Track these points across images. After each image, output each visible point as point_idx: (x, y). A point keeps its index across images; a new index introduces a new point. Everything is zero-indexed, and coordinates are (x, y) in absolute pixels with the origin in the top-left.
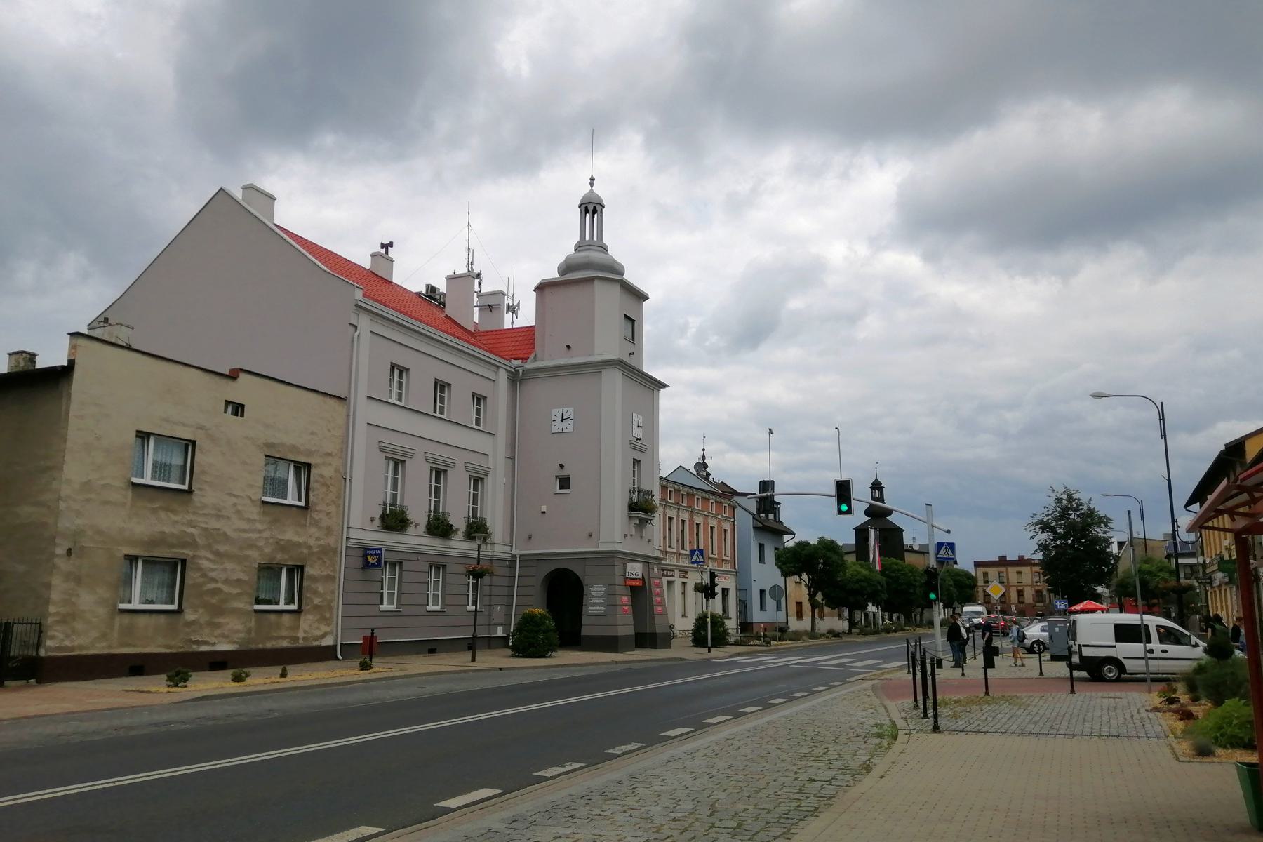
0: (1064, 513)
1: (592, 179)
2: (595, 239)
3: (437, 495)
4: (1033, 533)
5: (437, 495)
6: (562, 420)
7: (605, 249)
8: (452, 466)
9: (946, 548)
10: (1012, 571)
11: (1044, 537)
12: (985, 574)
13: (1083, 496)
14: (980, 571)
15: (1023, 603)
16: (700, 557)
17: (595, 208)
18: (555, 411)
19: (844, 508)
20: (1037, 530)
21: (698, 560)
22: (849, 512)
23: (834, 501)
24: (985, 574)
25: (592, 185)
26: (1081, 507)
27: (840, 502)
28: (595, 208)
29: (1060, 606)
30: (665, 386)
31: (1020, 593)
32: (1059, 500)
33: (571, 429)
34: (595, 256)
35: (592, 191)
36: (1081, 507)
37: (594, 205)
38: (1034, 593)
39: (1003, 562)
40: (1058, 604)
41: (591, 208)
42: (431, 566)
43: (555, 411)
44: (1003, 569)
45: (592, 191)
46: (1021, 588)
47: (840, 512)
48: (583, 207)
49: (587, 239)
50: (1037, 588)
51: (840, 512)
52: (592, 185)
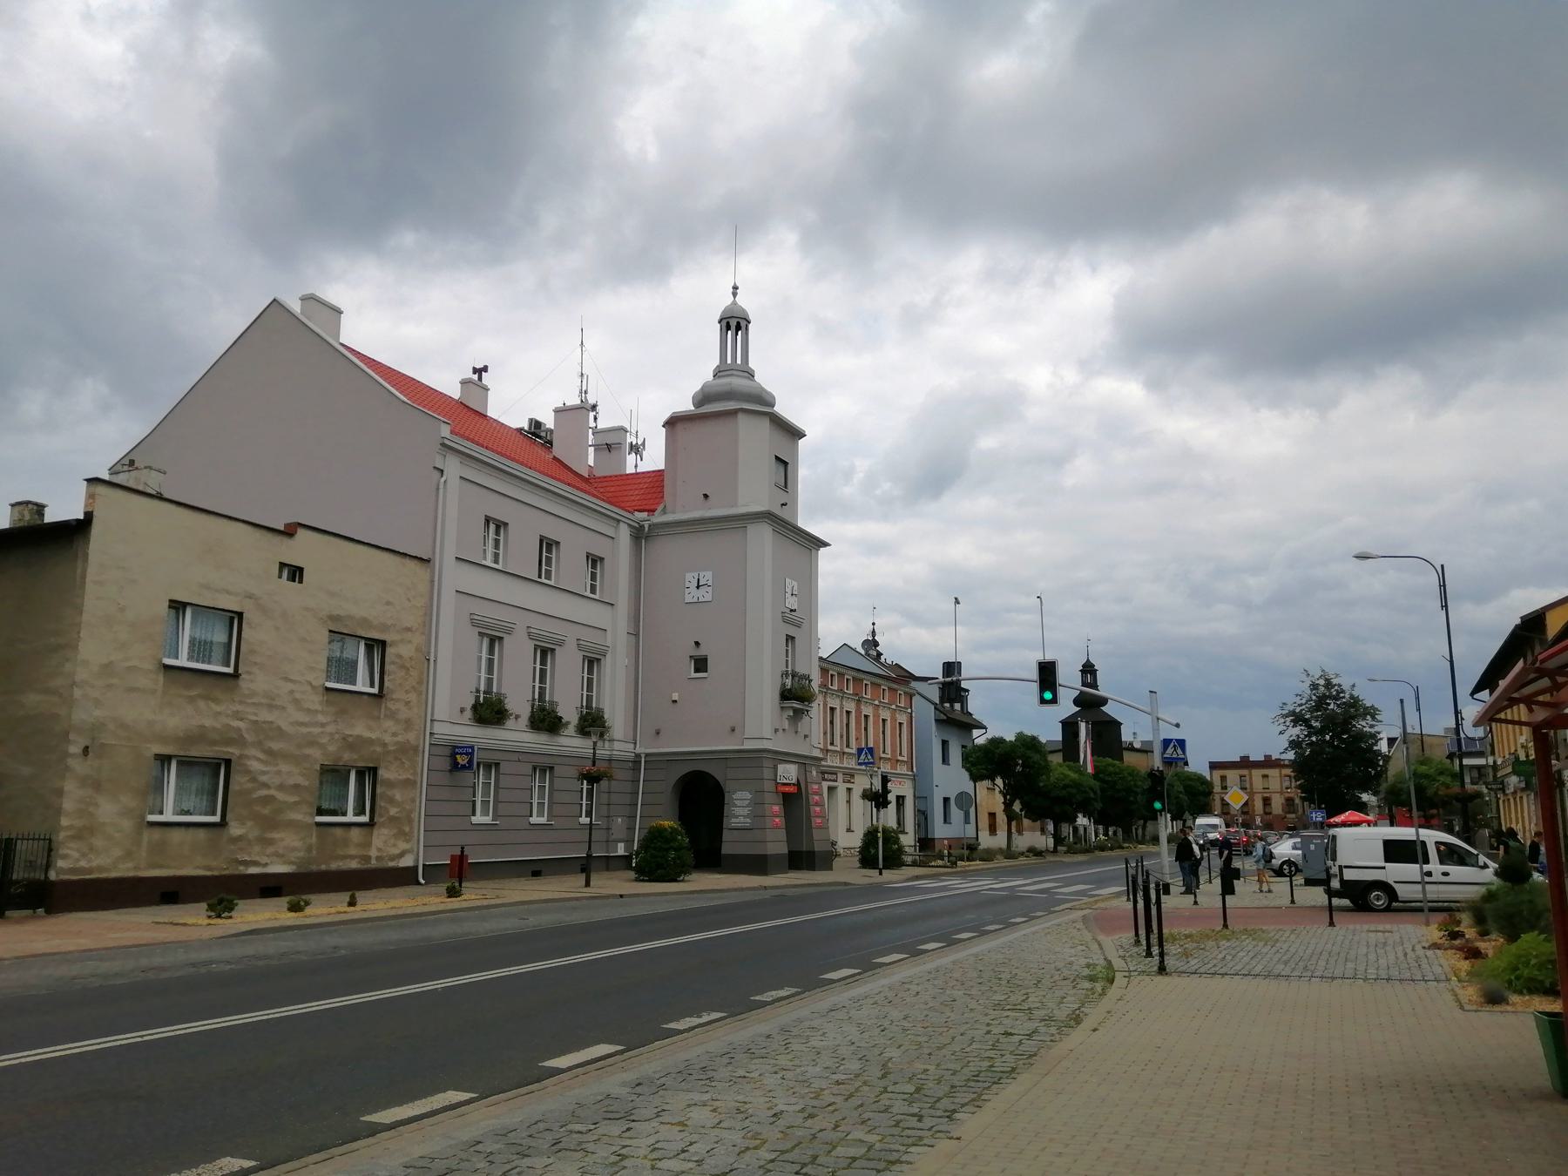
0: (1321, 703)
2: (739, 362)
3: (542, 680)
4: (1282, 728)
5: (542, 680)
6: (698, 587)
7: (751, 375)
8: (561, 643)
10: (1257, 774)
11: (1296, 731)
12: (1223, 778)
13: (1345, 682)
16: (869, 757)
17: (738, 323)
18: (689, 576)
19: (1048, 696)
20: (1288, 724)
21: (866, 761)
22: (1054, 701)
23: (1035, 687)
25: (735, 294)
26: (1342, 695)
27: (1042, 689)
28: (738, 323)
30: (825, 544)
31: (1267, 802)
32: (1314, 686)
33: (708, 597)
34: (738, 382)
35: (734, 303)
36: (1342, 695)
38: (1284, 802)
40: (1314, 815)
41: (733, 324)
42: (535, 769)
43: (689, 576)
45: (734, 303)
46: (1268, 795)
47: (1043, 701)
48: (724, 323)
49: (729, 361)
50: (1287, 795)
51: (1043, 701)
52: (735, 294)
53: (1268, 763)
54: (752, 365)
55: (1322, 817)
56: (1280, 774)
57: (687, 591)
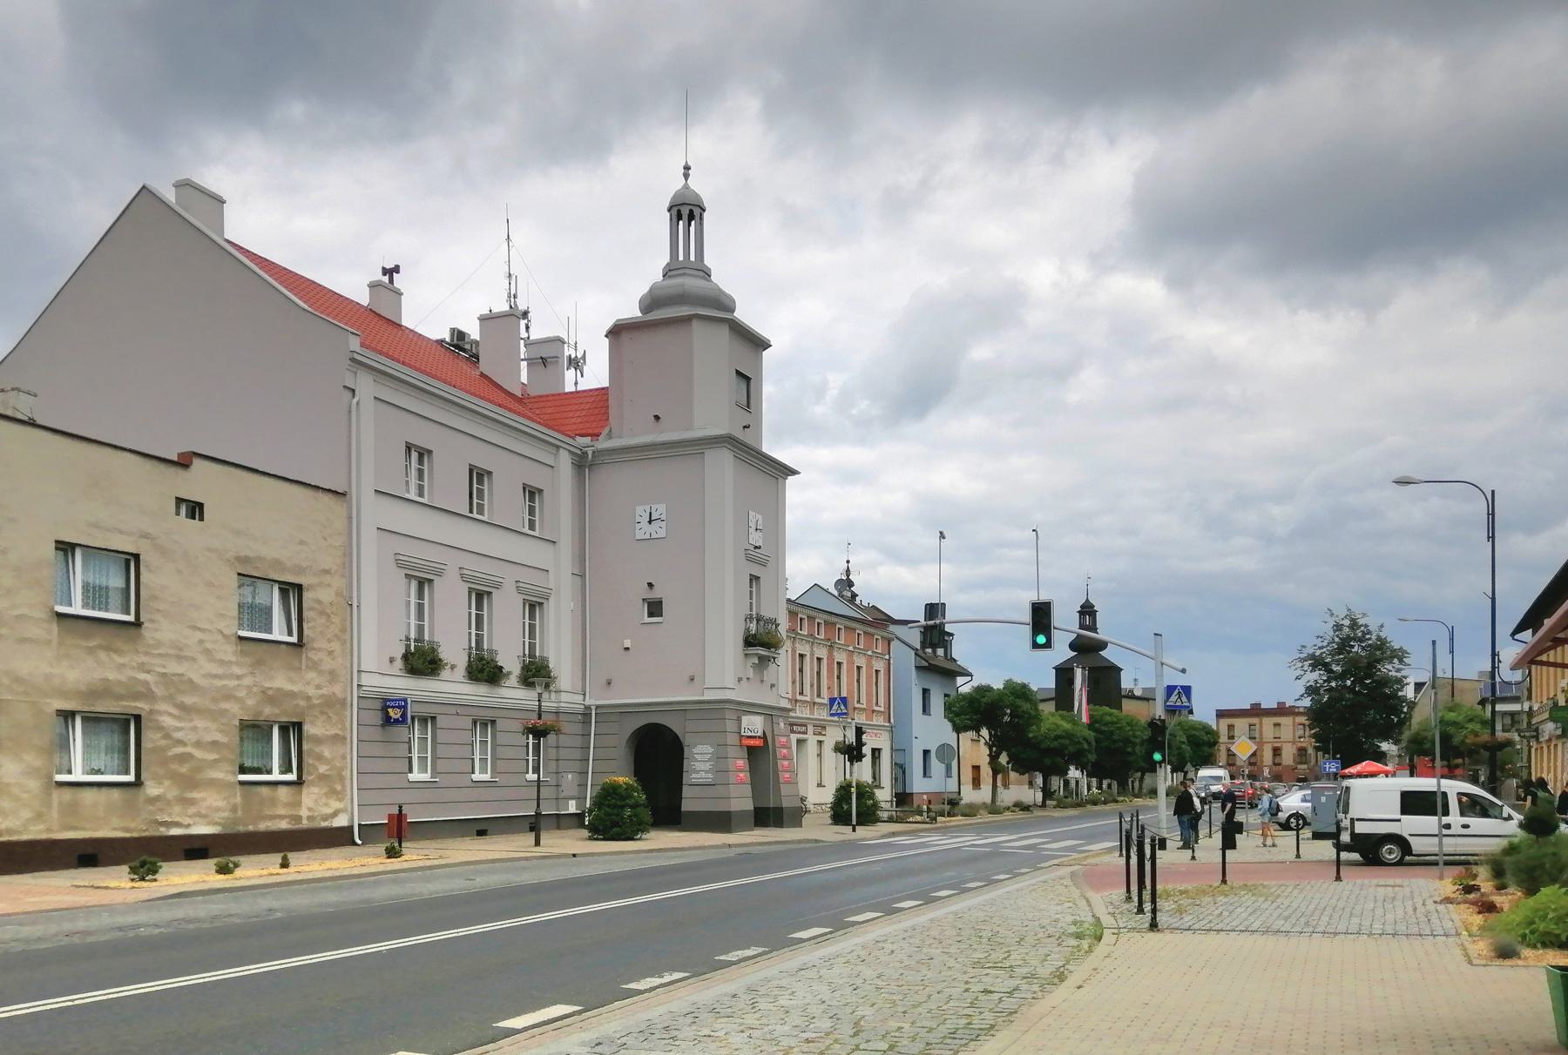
0: (1344, 645)
1: (687, 168)
2: (692, 258)
4: (1299, 672)
6: (650, 522)
7: (706, 274)
9: (839, 703)
10: (1268, 722)
11: (1315, 676)
12: (1231, 727)
14: (1225, 722)
15: (1280, 764)
16: (843, 707)
18: (639, 510)
19: (1041, 639)
20: (1305, 668)
22: (1048, 645)
23: (1028, 630)
24: (1231, 727)
25: (686, 176)
26: (1368, 636)
27: (1036, 632)
29: (1330, 768)
30: (794, 472)
31: (1277, 752)
33: (662, 534)
34: (692, 283)
35: (686, 187)
36: (1368, 636)
37: (691, 207)
38: (1295, 751)
39: (1256, 711)
40: (1327, 766)
41: (685, 212)
43: (639, 510)
44: (1255, 720)
45: (686, 187)
46: (1278, 745)
47: (1035, 645)
50: (1299, 745)
51: (1035, 645)
52: (686, 176)
53: (1282, 710)
54: (708, 261)
55: (1336, 768)
56: (1294, 722)
57: (638, 526)
